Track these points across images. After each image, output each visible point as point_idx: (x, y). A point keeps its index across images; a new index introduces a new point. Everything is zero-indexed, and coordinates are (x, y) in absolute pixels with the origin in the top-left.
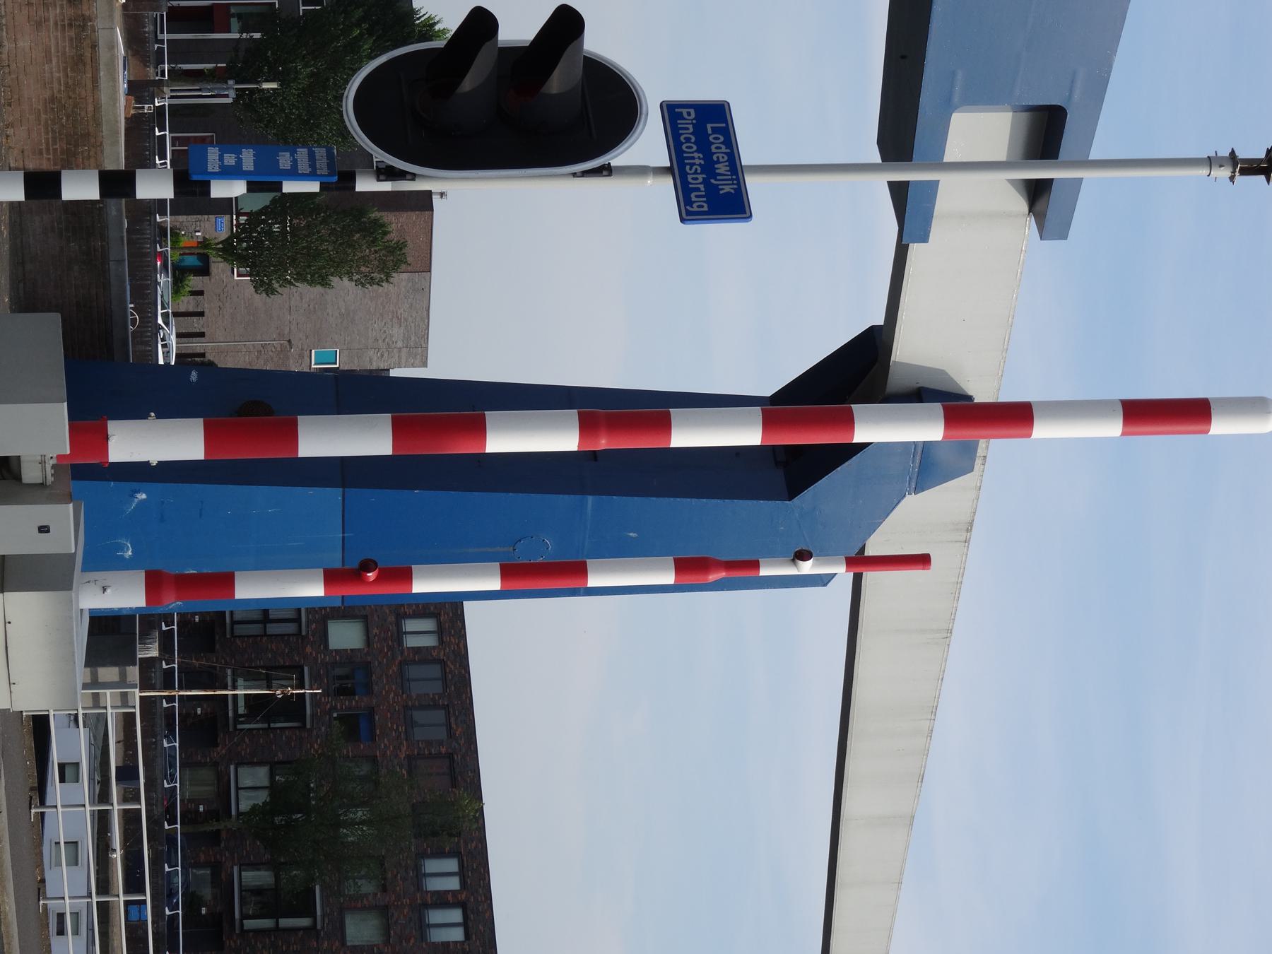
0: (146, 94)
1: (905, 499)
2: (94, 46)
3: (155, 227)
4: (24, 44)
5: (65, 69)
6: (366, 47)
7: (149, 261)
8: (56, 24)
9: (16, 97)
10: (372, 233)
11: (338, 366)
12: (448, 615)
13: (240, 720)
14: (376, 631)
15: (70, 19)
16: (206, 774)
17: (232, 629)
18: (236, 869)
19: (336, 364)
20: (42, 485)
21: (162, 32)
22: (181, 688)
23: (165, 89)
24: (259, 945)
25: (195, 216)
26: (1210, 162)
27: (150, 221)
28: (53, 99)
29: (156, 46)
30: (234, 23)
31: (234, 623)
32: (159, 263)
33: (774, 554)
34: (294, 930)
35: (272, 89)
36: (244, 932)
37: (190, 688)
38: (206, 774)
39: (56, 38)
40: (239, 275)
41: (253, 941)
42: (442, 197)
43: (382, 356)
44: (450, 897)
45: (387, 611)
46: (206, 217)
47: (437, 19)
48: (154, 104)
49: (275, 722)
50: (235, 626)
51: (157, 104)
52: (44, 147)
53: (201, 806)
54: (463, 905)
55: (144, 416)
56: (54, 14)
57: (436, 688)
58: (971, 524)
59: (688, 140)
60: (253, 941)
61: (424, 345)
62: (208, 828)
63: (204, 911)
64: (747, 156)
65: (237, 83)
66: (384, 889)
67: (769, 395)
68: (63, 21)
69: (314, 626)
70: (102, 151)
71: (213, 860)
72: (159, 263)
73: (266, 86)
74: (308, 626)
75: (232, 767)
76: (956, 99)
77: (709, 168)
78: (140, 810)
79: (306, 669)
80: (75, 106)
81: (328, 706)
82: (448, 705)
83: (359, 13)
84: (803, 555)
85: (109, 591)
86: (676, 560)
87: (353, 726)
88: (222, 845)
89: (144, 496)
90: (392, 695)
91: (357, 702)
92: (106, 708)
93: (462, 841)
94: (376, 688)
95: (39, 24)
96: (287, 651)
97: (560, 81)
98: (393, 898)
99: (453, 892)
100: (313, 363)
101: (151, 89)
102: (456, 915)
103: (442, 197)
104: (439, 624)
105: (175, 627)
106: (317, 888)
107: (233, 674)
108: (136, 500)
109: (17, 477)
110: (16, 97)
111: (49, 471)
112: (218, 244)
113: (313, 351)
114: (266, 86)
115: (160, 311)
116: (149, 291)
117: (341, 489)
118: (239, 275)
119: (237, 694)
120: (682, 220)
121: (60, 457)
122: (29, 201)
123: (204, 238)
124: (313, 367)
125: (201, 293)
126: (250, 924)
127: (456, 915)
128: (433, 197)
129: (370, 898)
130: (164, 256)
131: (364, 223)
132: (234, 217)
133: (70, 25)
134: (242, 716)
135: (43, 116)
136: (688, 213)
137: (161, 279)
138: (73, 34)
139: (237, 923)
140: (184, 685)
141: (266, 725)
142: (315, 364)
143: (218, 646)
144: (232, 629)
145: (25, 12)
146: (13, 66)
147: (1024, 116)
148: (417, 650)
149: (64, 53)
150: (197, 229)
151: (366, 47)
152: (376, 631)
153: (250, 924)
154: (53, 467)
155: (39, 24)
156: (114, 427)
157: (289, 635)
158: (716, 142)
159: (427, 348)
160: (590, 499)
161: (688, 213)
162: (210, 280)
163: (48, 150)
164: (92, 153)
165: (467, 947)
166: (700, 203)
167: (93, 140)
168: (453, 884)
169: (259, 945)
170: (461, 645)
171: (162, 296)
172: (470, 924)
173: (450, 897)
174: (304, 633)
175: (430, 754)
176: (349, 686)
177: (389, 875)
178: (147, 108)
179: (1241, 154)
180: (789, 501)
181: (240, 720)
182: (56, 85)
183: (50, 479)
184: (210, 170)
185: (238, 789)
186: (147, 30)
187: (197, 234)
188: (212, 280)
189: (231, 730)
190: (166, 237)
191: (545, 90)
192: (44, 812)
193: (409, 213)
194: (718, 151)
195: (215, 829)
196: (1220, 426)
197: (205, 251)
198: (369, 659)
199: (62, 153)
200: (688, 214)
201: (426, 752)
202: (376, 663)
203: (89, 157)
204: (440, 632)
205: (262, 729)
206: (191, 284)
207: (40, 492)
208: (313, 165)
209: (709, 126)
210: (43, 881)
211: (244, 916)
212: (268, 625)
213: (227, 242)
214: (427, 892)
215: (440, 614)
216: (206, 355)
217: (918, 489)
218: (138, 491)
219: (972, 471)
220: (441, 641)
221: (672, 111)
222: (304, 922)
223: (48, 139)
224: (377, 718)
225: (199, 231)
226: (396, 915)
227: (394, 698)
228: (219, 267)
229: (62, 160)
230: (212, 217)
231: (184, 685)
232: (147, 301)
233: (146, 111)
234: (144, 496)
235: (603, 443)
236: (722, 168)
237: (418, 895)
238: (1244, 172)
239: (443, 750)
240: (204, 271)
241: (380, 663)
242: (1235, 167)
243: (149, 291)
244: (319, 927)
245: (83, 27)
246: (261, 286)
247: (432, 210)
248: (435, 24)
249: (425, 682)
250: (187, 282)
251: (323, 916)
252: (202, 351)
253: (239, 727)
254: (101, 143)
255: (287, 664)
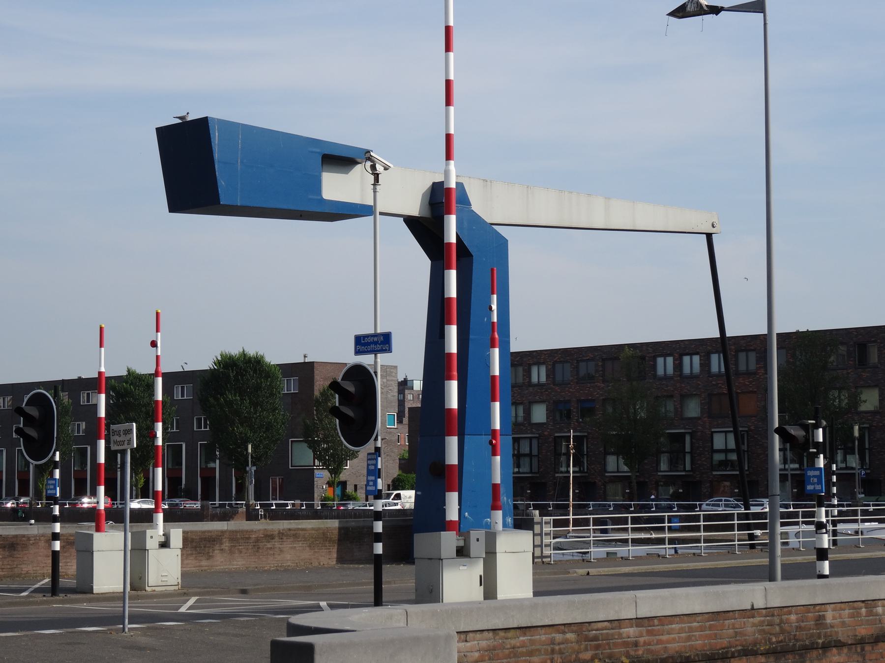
0: (253, 513)
1: (473, 210)
2: (290, 530)
3: (323, 510)
4: (288, 557)
5: (298, 541)
6: (230, 397)
7: (342, 514)
8: (281, 544)
9: (308, 561)
10: (328, 395)
11: (396, 414)
12: (529, 359)
13: (582, 469)
14: (537, 398)
15: (280, 539)
16: (610, 488)
17: (534, 473)
18: (659, 474)
19: (394, 415)
20: (465, 540)
21: (215, 504)
22: (569, 500)
23: (251, 503)
24: (699, 462)
25: (315, 488)
26: (375, 192)
27: (321, 512)
28: (310, 546)
29: (227, 507)
30: (212, 465)
31: (531, 472)
32: (342, 508)
33: (490, 317)
34: (692, 444)
35: (252, 446)
36: (692, 470)
37: (569, 496)
38: (610, 488)
39: (287, 544)
40: (347, 466)
41: (697, 465)
42: (306, 357)
43: (390, 390)
44: (677, 362)
45: (527, 391)
46: (315, 483)
47: (215, 359)
48: (259, 509)
49: (584, 452)
50: (533, 471)
51: (259, 507)
52: (328, 550)
53: (627, 491)
54: (681, 355)
55: (445, 509)
56: (277, 545)
57: (567, 366)
58: (484, 180)
59: (367, 348)
60: (697, 465)
61: (385, 368)
62: (635, 487)
63: (681, 491)
64: (372, 332)
65: (248, 466)
66: (672, 396)
67: (430, 262)
68: (280, 541)
69: (534, 430)
70: (330, 528)
71: (655, 486)
72: (342, 508)
73: (250, 450)
74: (534, 433)
75: (607, 474)
76: (319, 198)
77: (376, 343)
78: (593, 518)
79: (556, 435)
80: (312, 538)
81: (576, 423)
82: (577, 361)
83: (211, 400)
84: (491, 308)
85: (497, 522)
86: (491, 348)
87: (587, 410)
88: (647, 480)
89: (467, 513)
90: (571, 390)
91: (574, 409)
92: (551, 531)
93: (648, 355)
94: (567, 398)
95: (281, 551)
96: (547, 445)
97: (350, 387)
98: (676, 392)
99: (674, 360)
100: (394, 427)
101: (250, 510)
102: (686, 360)
103: (306, 357)
104: (535, 364)
105: (532, 503)
106: (668, 431)
107: (558, 473)
108: (468, 517)
109: (462, 547)
110: (308, 561)
111: (460, 538)
112: (332, 477)
113: (388, 427)
114: (250, 450)
115: (368, 508)
116: (341, 513)
117: (465, 436)
118: (347, 466)
119: (573, 471)
120: (391, 352)
121: (457, 535)
122: (382, 540)
123: (326, 484)
124: (396, 427)
125: (356, 486)
126: (688, 467)
127: (686, 360)
128: (306, 361)
129: (676, 404)
130: (339, 505)
131: (322, 400)
132: (315, 467)
133: (282, 539)
134: (580, 469)
135: (316, 550)
136: (389, 350)
137: (350, 507)
138: (285, 538)
139: (687, 473)
140: (199, 497)
141: (585, 457)
142: (395, 426)
143: (543, 481)
144: (534, 473)
145: (276, 556)
146: (297, 562)
147: (324, 167)
148: (548, 376)
149: (292, 541)
150: (322, 487)
151: (230, 397)
152: (537, 398)
153: (688, 467)
154: (459, 537)
155: (281, 551)
156: (448, 519)
157: (538, 443)
158: (367, 340)
159: (387, 366)
160: (471, 337)
161: (389, 350)
162: (348, 481)
163: (329, 549)
164: (330, 532)
165: (702, 354)
166: (386, 347)
167: (326, 531)
168: (670, 360)
169: (699, 462)
170: (546, 353)
171: (360, 506)
172: (691, 352)
173: (677, 362)
174: (538, 436)
175: (602, 370)
176: (565, 412)
177: (665, 394)
178: (261, 512)
179: (373, 183)
180: (473, 256)
181: (582, 469)
182: (304, 545)
183: (463, 538)
184: (374, 489)
185: (618, 472)
186: (219, 512)
187: (324, 487)
188: (349, 480)
189: (587, 475)
190: (326, 504)
191: (354, 393)
192: (545, 533)
193: (315, 375)
194: (370, 340)
195: (635, 484)
196: (452, 131)
197: (336, 484)
198: (552, 401)
199: (330, 543)
200: (389, 350)
201: (601, 372)
202: (554, 398)
203: (332, 533)
204: (539, 364)
205: (587, 458)
206: (351, 491)
207: (467, 540)
208: (373, 459)
209: (362, 342)
210: (622, 558)
211: (685, 470)
212: (533, 454)
213: (331, 472)
214: (674, 374)
215: (529, 364)
216: (389, 484)
217: (470, 204)
218: (465, 516)
219: (462, 183)
220: (543, 363)
221: (358, 352)
222: (688, 439)
223: (325, 549)
224: (583, 398)
225: (323, 487)
226: (686, 391)
227: (573, 389)
228: (343, 477)
229: (333, 543)
230: (315, 479)
231: (199, 497)
232: (363, 514)
233: (263, 513)
234: (467, 513)
235: (455, 373)
236: (376, 339)
237: (676, 379)
238: (378, 182)
239: (600, 364)
240: (344, 484)
241: (554, 396)
242: (376, 185)
243: (341, 513)
244: (690, 431)
245: (283, 534)
246: (355, 455)
247: (314, 362)
248: (218, 360)
249: (565, 372)
250: (350, 494)
251: (685, 429)
252: (387, 486)
253: (586, 470)
254: (327, 528)
255: (553, 444)
